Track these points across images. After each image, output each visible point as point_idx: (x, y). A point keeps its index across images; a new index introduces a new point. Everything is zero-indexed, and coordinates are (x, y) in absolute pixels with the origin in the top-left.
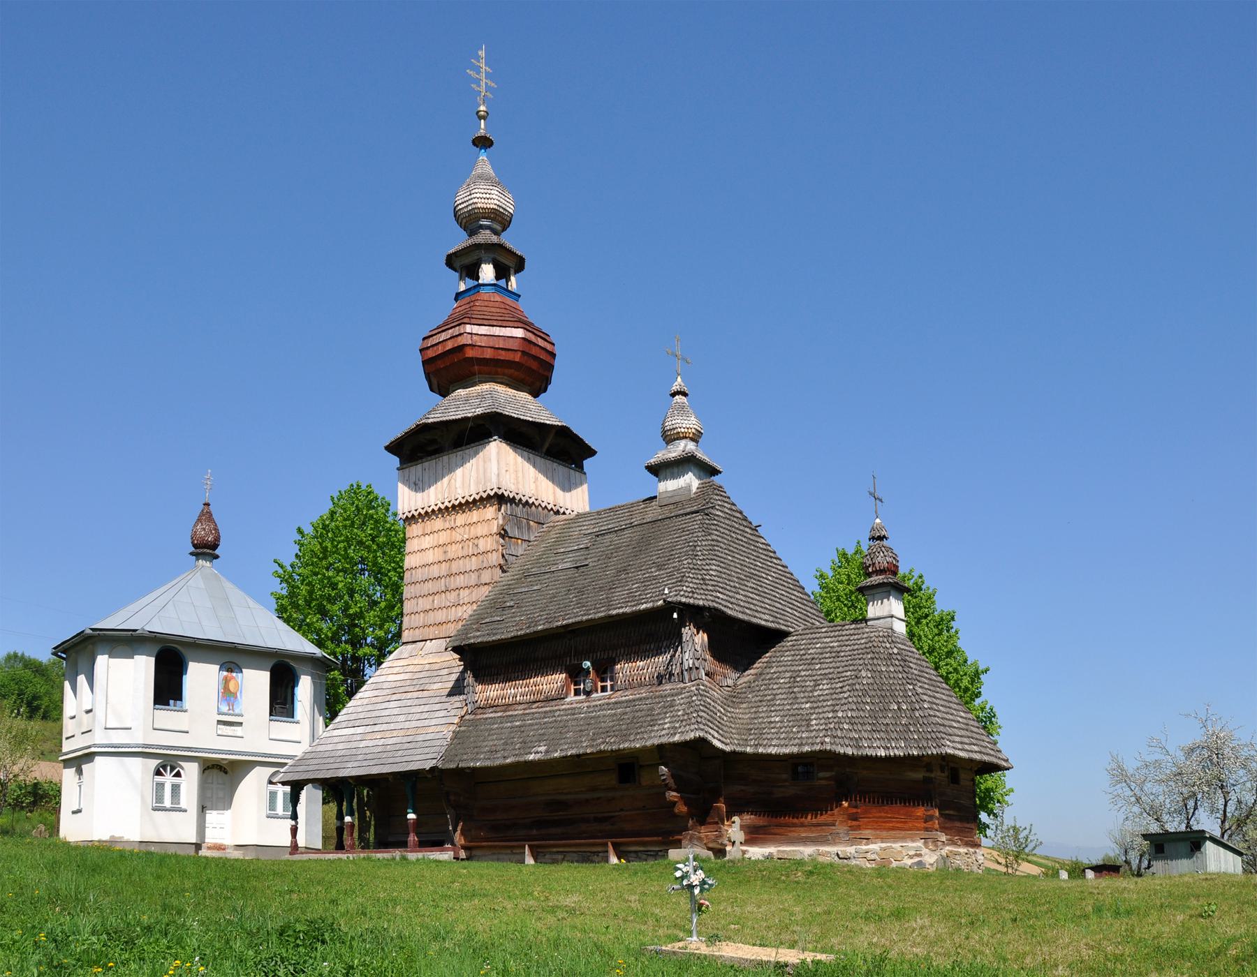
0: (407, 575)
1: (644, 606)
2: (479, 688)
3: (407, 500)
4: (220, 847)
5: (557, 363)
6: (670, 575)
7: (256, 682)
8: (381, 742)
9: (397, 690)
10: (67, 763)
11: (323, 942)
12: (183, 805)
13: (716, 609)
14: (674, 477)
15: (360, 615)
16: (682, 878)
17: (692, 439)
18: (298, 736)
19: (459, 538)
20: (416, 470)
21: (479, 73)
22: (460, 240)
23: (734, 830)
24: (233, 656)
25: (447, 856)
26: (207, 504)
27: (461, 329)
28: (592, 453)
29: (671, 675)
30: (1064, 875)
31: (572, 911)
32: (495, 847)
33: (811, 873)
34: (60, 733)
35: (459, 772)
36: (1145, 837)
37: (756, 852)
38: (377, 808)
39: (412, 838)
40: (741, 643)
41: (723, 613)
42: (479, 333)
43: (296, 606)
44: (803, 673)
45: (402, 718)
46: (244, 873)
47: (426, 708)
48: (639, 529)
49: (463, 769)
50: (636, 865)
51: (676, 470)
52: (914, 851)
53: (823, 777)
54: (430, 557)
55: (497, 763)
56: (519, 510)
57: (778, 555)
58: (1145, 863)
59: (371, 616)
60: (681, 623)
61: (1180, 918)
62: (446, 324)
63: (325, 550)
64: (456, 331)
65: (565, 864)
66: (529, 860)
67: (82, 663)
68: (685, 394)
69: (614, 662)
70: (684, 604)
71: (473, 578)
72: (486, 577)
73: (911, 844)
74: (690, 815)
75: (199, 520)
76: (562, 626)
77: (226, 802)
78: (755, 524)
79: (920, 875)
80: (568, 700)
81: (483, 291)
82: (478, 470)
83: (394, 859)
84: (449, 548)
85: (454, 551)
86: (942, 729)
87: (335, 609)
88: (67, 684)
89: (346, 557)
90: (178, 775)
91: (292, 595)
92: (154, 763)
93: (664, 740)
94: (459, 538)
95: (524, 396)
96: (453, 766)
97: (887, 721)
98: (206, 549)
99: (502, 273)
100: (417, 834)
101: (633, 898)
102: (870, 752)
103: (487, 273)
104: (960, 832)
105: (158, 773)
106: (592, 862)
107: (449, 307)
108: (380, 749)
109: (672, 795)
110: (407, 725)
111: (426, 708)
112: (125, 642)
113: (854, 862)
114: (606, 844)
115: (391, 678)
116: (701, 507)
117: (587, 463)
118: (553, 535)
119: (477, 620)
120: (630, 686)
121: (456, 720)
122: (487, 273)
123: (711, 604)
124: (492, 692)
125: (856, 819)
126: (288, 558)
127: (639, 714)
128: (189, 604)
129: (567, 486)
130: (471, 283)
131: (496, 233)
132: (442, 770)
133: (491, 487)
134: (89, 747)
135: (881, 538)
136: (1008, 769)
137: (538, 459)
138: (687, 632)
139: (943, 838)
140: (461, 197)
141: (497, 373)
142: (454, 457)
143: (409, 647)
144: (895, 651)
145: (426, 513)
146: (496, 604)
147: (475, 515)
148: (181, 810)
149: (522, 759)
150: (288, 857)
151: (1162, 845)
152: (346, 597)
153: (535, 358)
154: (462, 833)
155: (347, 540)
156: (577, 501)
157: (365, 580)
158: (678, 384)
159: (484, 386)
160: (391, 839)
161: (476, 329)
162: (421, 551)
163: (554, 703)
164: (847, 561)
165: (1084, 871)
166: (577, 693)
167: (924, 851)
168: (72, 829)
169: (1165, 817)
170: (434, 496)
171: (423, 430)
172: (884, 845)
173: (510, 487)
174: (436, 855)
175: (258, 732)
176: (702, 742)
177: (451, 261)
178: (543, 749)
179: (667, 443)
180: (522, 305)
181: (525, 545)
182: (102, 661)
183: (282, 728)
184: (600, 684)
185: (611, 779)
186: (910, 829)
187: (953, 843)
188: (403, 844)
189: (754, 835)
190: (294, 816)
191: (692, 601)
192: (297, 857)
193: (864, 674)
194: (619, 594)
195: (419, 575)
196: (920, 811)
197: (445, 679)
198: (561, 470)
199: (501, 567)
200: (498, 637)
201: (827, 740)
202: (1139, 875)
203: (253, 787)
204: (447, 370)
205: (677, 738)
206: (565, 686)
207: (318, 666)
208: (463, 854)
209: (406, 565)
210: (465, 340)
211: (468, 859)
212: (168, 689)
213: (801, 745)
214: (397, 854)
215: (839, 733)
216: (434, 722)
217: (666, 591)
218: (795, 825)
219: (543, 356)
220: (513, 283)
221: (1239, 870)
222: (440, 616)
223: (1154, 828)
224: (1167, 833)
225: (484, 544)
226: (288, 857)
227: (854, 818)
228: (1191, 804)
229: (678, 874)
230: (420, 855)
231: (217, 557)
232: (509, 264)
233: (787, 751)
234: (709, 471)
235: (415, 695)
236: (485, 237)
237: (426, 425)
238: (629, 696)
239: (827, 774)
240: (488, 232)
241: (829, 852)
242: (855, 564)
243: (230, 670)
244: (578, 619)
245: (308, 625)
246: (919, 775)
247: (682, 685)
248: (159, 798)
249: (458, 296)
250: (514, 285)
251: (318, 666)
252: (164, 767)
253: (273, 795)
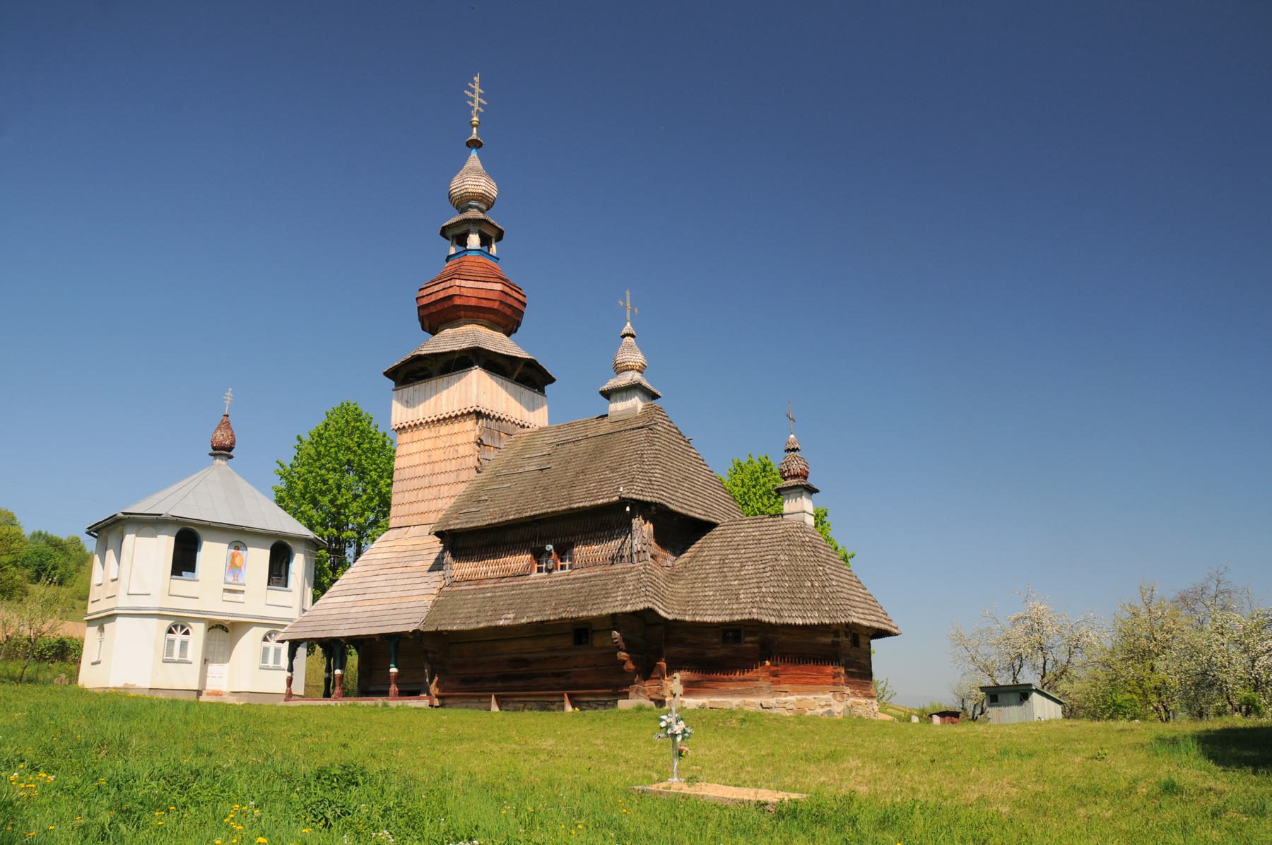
2: (456, 565)
3: (400, 413)
4: (218, 694)
5: (526, 311)
6: (623, 477)
7: (259, 558)
8: (370, 608)
10: (90, 622)
11: (357, 784)
12: (189, 658)
14: (622, 400)
15: (346, 506)
16: (667, 727)
18: (291, 602)
19: (444, 445)
20: (408, 391)
23: (675, 683)
24: (239, 536)
27: (452, 283)
28: (552, 380)
29: (622, 557)
30: (915, 719)
31: (550, 754)
33: (744, 720)
35: (437, 635)
36: (982, 689)
37: (692, 702)
38: (373, 664)
39: (393, 688)
40: (679, 531)
42: (467, 288)
43: (292, 497)
45: (388, 589)
46: (247, 717)
47: (410, 581)
50: (589, 713)
52: (823, 701)
53: (749, 641)
54: (416, 459)
55: (472, 627)
56: (493, 424)
58: (978, 711)
59: (354, 506)
60: (632, 515)
61: (1078, 760)
63: (319, 453)
65: (527, 712)
66: (495, 708)
67: (112, 540)
68: (633, 336)
69: (572, 546)
71: (452, 478)
72: (464, 476)
73: (822, 696)
74: (637, 672)
75: (219, 428)
76: (530, 517)
77: (226, 656)
79: (830, 721)
80: (532, 576)
81: (469, 254)
83: (376, 706)
84: (433, 453)
85: (436, 455)
87: (325, 500)
88: (97, 558)
89: (337, 459)
90: (187, 633)
91: (290, 488)
92: (167, 623)
93: (618, 610)
94: (442, 445)
95: (500, 336)
96: (432, 629)
98: (223, 451)
99: (485, 241)
100: (397, 685)
101: (598, 742)
102: (790, 621)
103: (474, 241)
104: (860, 686)
105: (170, 631)
106: (549, 710)
109: (623, 655)
110: (393, 595)
111: (410, 581)
112: (151, 523)
113: (775, 711)
115: (379, 556)
116: (646, 425)
118: (520, 444)
119: (457, 511)
120: (586, 565)
121: (436, 591)
122: (474, 241)
123: (658, 501)
124: (466, 568)
125: (776, 676)
126: (288, 460)
128: (208, 494)
129: (532, 407)
130: (462, 249)
131: (481, 211)
132: (422, 633)
135: (794, 450)
137: (509, 384)
138: (637, 522)
139: (848, 690)
143: (395, 531)
146: (473, 498)
147: (456, 427)
149: (493, 624)
150: (283, 703)
151: (995, 695)
152: (335, 491)
153: (510, 306)
154: (437, 686)
155: (338, 446)
156: (539, 418)
157: (351, 478)
158: (628, 328)
160: (372, 689)
161: (463, 283)
162: (409, 455)
164: (742, 469)
165: (931, 716)
166: (540, 570)
167: (833, 702)
168: (89, 677)
169: (996, 673)
173: (486, 407)
174: (413, 703)
176: (650, 611)
177: (444, 232)
178: (511, 616)
181: (496, 451)
182: (129, 539)
183: (278, 595)
184: (559, 563)
185: (568, 641)
187: (856, 696)
188: (385, 693)
189: (691, 688)
190: (291, 669)
192: (291, 703)
193: (782, 557)
194: (579, 492)
195: (407, 474)
196: (829, 669)
197: (426, 557)
198: (527, 393)
202: (974, 719)
203: (249, 643)
204: (437, 316)
205: (629, 608)
206: (530, 565)
207: (312, 545)
208: (437, 702)
211: (442, 706)
212: (184, 561)
213: (732, 614)
214: (379, 701)
216: (416, 593)
218: (724, 680)
219: (516, 305)
220: (494, 249)
221: (1060, 715)
222: (423, 507)
223: (988, 682)
224: (998, 686)
225: (463, 450)
226: (283, 703)
227: (775, 674)
228: (1017, 663)
229: (663, 724)
230: (400, 703)
233: (720, 619)
235: (400, 570)
236: (473, 214)
237: (419, 356)
238: (585, 573)
239: (752, 639)
241: (752, 702)
242: (747, 471)
243: (237, 548)
245: (302, 512)
246: (828, 640)
248: (170, 651)
249: (449, 258)
251: (312, 545)
252: (176, 627)
253: (266, 651)
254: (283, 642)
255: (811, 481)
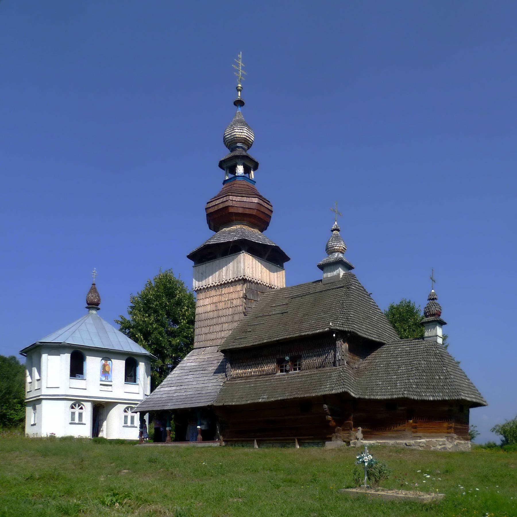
0: (197, 317)
1: (318, 331)
5: (273, 215)
6: (331, 317)
7: (119, 366)
9: (192, 370)
12: (83, 422)
13: (353, 332)
17: (341, 252)
21: (238, 66)
22: (226, 154)
24: (107, 354)
25: (216, 444)
26: (94, 284)
32: (238, 441)
34: (25, 391)
40: (363, 347)
41: (357, 334)
42: (235, 201)
44: (392, 362)
48: (313, 295)
49: (226, 406)
51: (332, 267)
52: (441, 442)
54: (209, 308)
57: (379, 307)
60: (336, 339)
62: (219, 195)
64: (225, 199)
66: (256, 446)
67: (35, 357)
68: (338, 230)
70: (339, 330)
72: (236, 318)
75: (90, 292)
78: (369, 293)
81: (238, 179)
82: (234, 267)
85: (221, 306)
86: (459, 387)
90: (81, 408)
92: (71, 403)
95: (256, 231)
96: (221, 404)
97: (434, 384)
98: (93, 305)
99: (247, 170)
102: (426, 398)
103: (240, 170)
105: (72, 408)
107: (220, 187)
108: (184, 397)
109: (329, 417)
112: (56, 348)
114: (294, 440)
116: (346, 285)
117: (285, 264)
119: (233, 338)
122: (240, 170)
127: (314, 381)
128: (86, 331)
133: (240, 276)
134: (39, 396)
135: (433, 299)
136: (485, 405)
138: (339, 343)
139: (455, 436)
140: (228, 132)
141: (244, 220)
142: (225, 259)
143: (197, 350)
144: (438, 352)
145: (207, 287)
146: (243, 330)
148: (83, 424)
159: (235, 225)
161: (234, 198)
162: (204, 305)
163: (270, 376)
167: (447, 442)
170: (211, 280)
171: (207, 247)
172: (428, 440)
175: (119, 389)
177: (222, 164)
179: (329, 254)
180: (256, 186)
183: (131, 387)
186: (441, 433)
191: (342, 328)
195: (203, 317)
196: (446, 425)
198: (274, 267)
199: (244, 313)
200: (244, 345)
201: (405, 392)
204: (218, 218)
205: (333, 392)
208: (223, 444)
209: (197, 312)
210: (230, 203)
212: (77, 369)
215: (411, 389)
217: (331, 324)
227: (415, 427)
231: (98, 309)
232: (251, 165)
233: (385, 397)
234: (348, 267)
235: (201, 372)
236: (237, 152)
237: (209, 246)
238: (308, 372)
240: (240, 149)
244: (286, 337)
246: (446, 408)
247: (335, 368)
249: (225, 182)
250: (253, 177)
252: (75, 405)
254: (136, 412)
255: (443, 317)
